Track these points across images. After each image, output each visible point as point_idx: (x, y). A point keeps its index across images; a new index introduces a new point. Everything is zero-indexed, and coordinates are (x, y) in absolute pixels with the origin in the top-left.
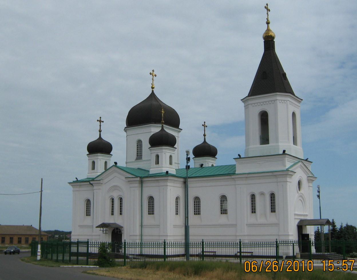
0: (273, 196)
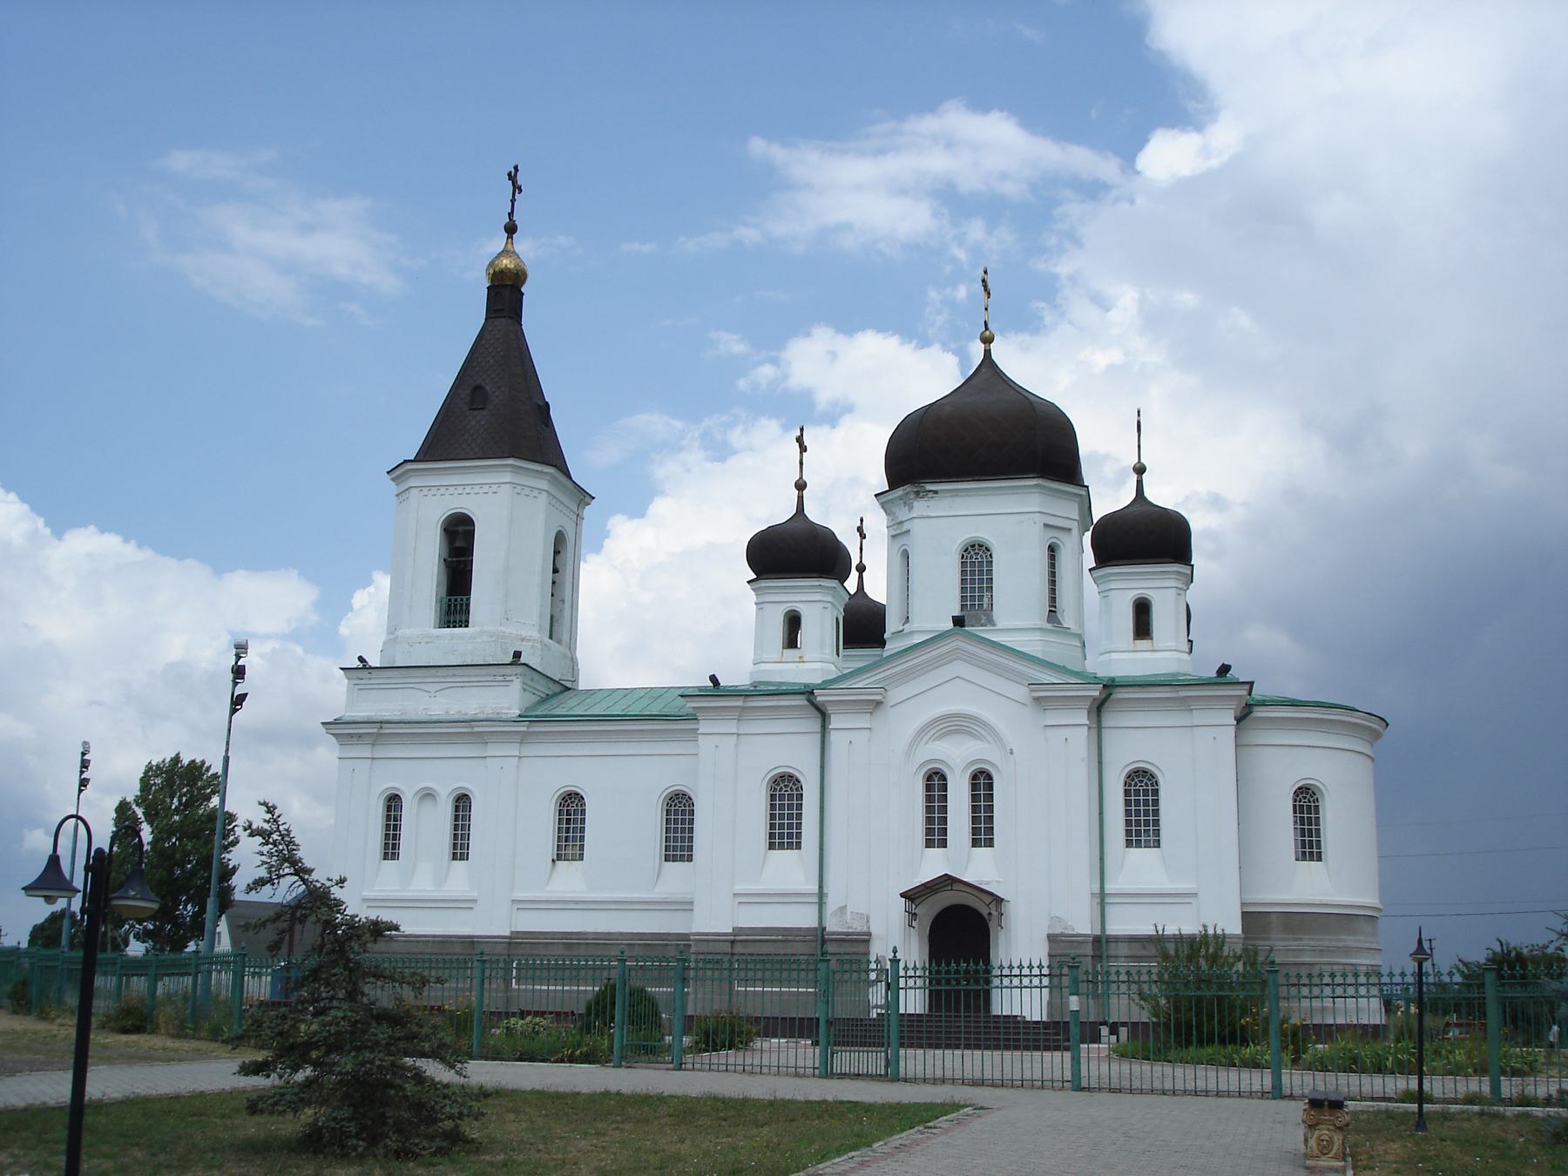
0: (462, 803)
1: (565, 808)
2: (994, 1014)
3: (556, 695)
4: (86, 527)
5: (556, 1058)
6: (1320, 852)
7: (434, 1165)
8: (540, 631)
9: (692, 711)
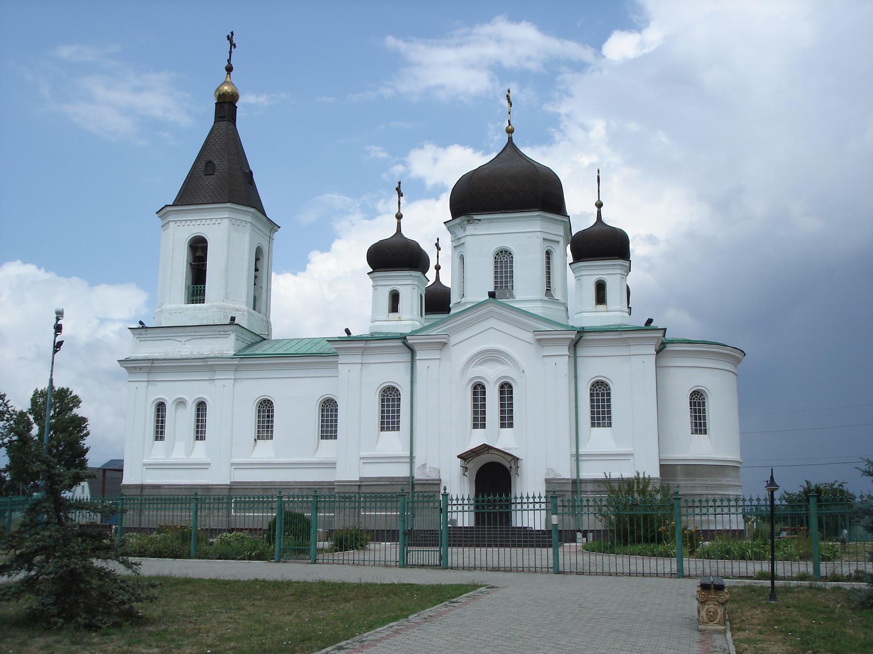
0: (201, 406)
1: (262, 409)
3: (257, 343)
4: (15, 261)
5: (240, 557)
6: (706, 429)
7: (109, 634)
8: (247, 304)
9: (335, 350)
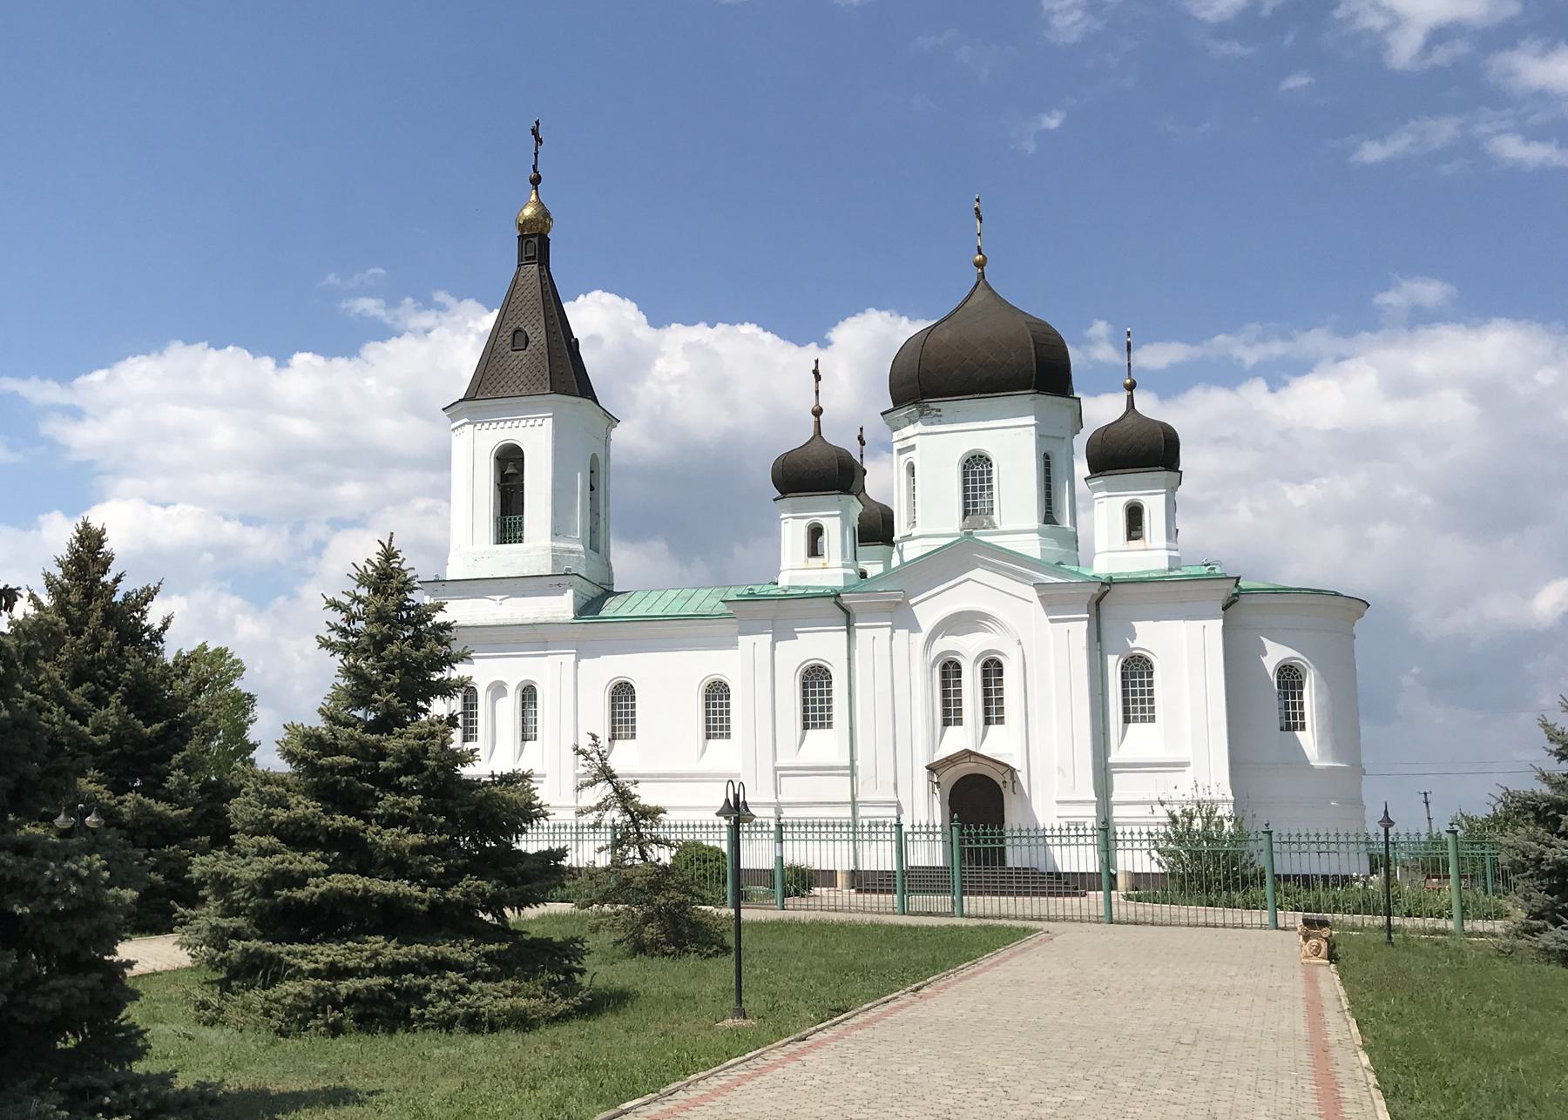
2: (1008, 866)
